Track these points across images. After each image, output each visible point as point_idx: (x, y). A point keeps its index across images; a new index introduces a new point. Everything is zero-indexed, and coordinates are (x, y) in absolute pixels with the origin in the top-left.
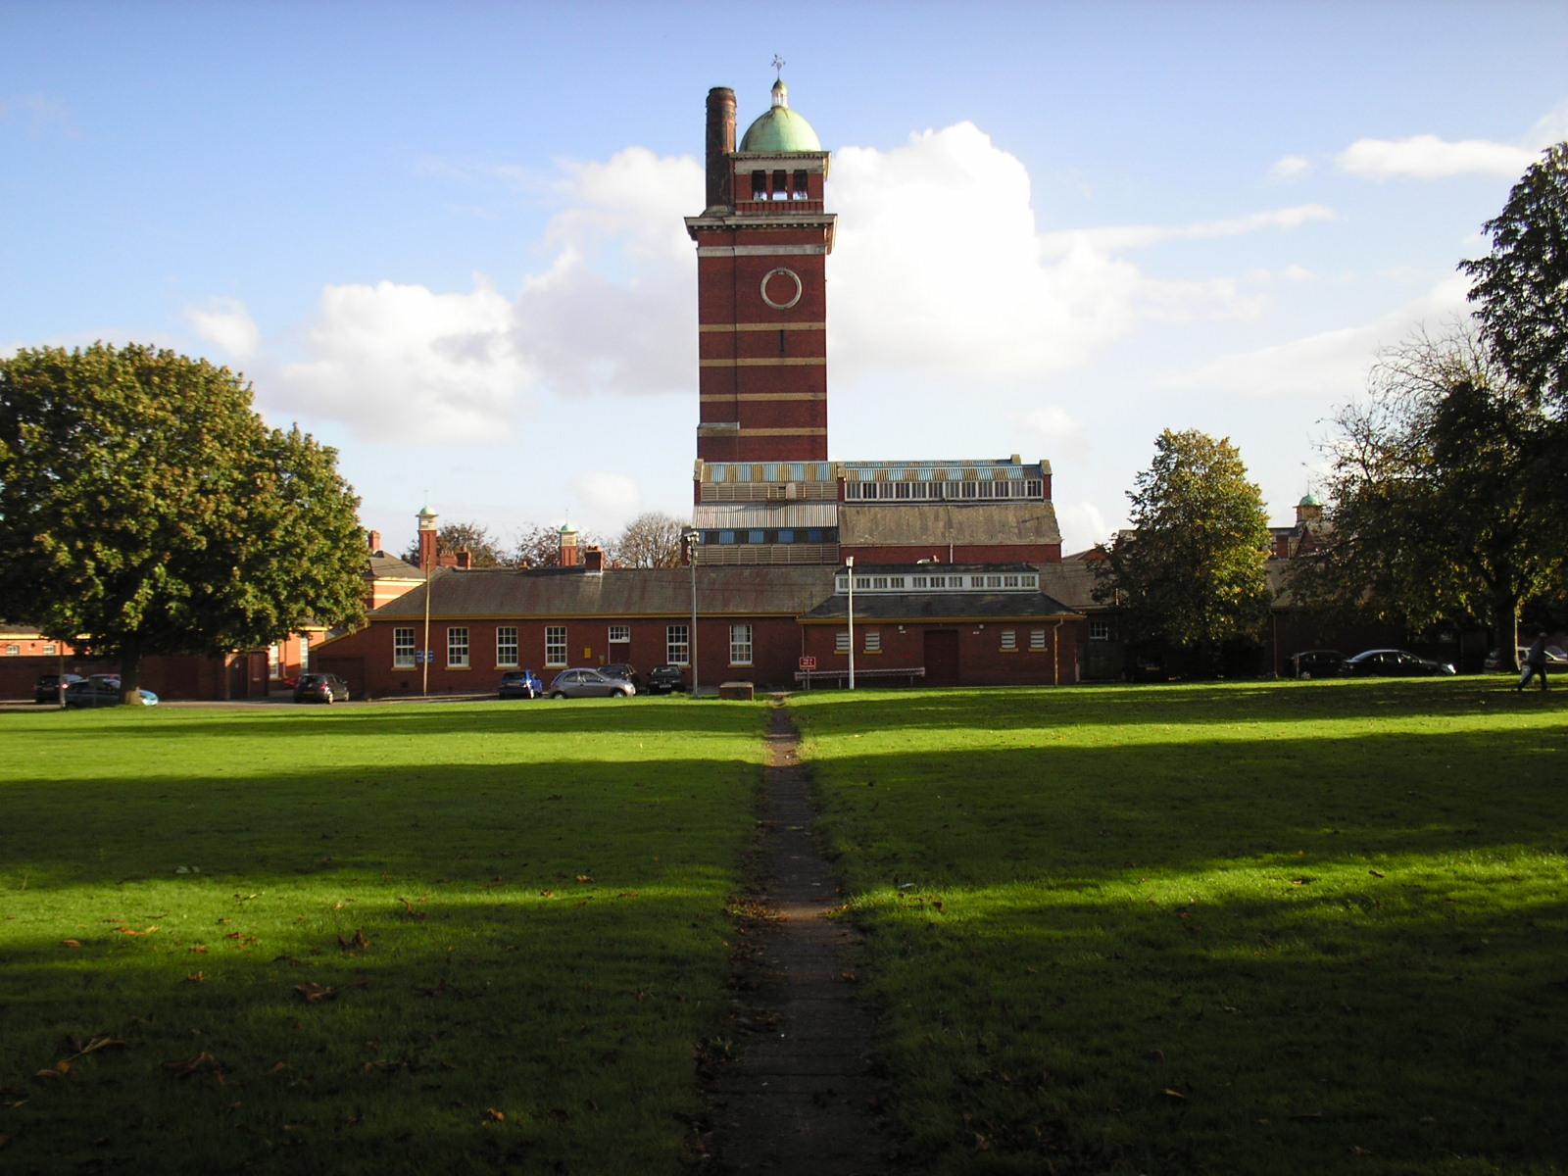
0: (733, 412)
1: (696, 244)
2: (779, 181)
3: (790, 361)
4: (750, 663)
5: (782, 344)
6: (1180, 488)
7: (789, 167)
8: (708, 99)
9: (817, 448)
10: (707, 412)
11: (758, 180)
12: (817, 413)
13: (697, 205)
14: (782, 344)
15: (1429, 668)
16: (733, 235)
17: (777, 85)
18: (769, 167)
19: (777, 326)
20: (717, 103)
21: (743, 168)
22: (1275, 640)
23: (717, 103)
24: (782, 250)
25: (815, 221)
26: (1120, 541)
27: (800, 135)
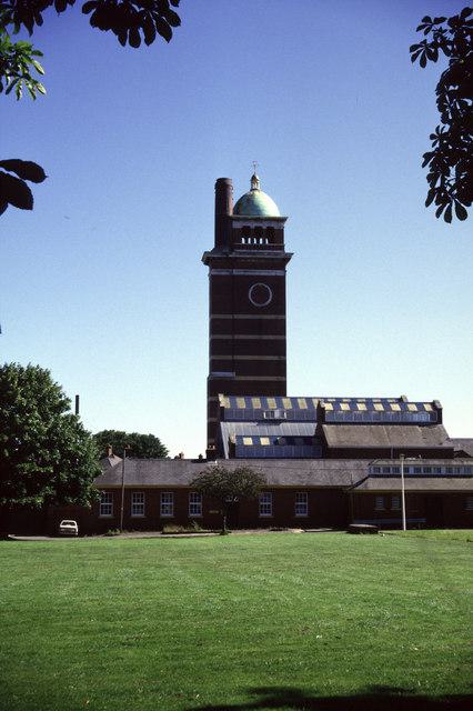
0: (231, 366)
1: (208, 267)
2: (258, 233)
3: (265, 337)
4: (306, 515)
5: (259, 327)
6: (51, 440)
7: (265, 226)
8: (216, 185)
9: (280, 389)
10: (214, 366)
11: (246, 232)
12: (280, 368)
13: (210, 245)
14: (259, 327)
15: (196, 527)
16: (233, 263)
17: (254, 178)
18: (253, 225)
19: (258, 317)
20: (222, 187)
21: (237, 225)
22: (403, 485)
23: (222, 187)
24: (264, 273)
25: (282, 256)
26: (179, 458)
27: (269, 207)
